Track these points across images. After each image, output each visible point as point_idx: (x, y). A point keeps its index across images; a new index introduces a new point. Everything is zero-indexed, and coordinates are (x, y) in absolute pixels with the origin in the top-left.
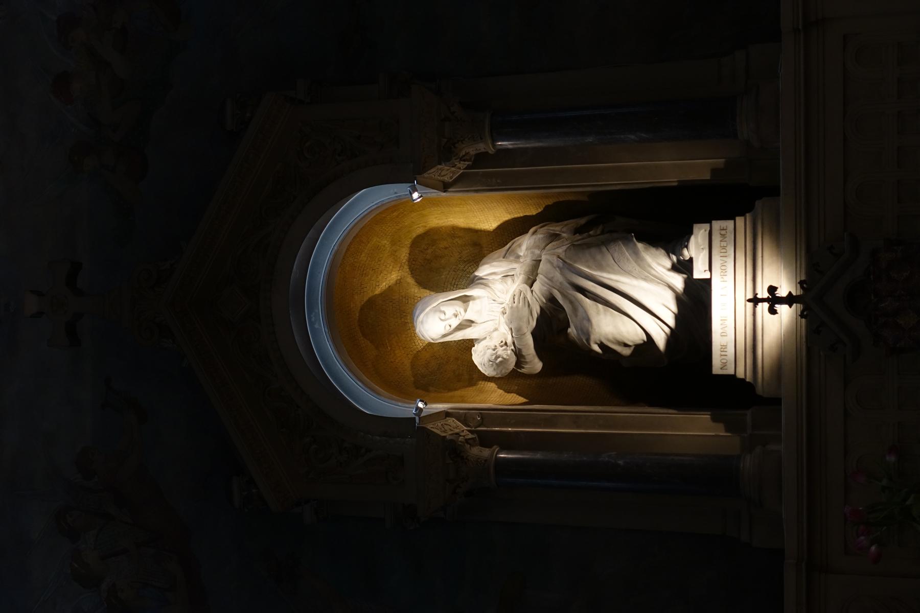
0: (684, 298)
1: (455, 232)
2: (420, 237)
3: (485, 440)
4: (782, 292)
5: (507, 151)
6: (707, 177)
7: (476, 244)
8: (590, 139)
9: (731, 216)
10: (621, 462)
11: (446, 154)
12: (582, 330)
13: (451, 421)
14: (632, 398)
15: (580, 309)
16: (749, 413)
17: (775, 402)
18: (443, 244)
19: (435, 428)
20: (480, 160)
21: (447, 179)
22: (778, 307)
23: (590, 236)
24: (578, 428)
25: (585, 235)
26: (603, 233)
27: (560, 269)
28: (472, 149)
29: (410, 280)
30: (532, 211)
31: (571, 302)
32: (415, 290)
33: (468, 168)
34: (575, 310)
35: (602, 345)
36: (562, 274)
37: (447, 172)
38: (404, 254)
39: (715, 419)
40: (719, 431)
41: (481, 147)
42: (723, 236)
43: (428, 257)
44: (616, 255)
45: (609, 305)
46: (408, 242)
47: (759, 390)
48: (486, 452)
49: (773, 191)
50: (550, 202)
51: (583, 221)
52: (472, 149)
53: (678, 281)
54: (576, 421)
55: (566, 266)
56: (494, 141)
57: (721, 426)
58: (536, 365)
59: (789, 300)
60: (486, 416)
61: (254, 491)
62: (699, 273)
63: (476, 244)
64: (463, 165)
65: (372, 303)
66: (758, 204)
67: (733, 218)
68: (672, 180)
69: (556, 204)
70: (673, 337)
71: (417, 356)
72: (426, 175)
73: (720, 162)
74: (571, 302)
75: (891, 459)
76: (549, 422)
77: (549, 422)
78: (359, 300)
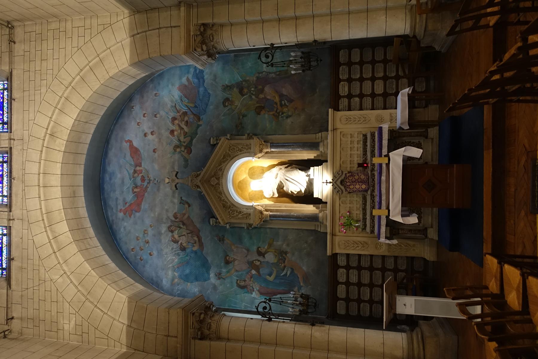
0: (308, 182)
1: (258, 167)
2: (251, 168)
3: (267, 210)
4: (328, 181)
5: (273, 151)
6: (313, 158)
7: (263, 170)
8: (290, 150)
9: (320, 166)
10: (295, 215)
11: (261, 151)
12: (287, 188)
13: (259, 206)
14: (296, 202)
15: (287, 184)
16: (320, 205)
17: (326, 203)
18: (255, 170)
19: (257, 207)
20: (267, 153)
21: (260, 156)
22: (327, 184)
23: (288, 169)
24: (286, 208)
25: (287, 169)
26: (291, 168)
27: (283, 175)
28: (265, 150)
29: (248, 177)
30: (276, 163)
31: (285, 182)
32: (249, 179)
33: (264, 154)
34: (286, 184)
35: (291, 192)
36: (283, 176)
37: (260, 155)
38: (247, 171)
39: (314, 206)
40: (315, 208)
41: (268, 150)
42: (316, 170)
43: (252, 172)
44: (295, 173)
45: (9, 244)
46: (248, 169)
47: (323, 201)
48: (267, 213)
49: (326, 161)
50: (280, 161)
51: (286, 166)
52: (265, 150)
53: (307, 178)
54: (286, 207)
55: (284, 175)
56: (270, 149)
57: (315, 208)
58: (276, 195)
59: (330, 183)
60: (266, 206)
61: (218, 221)
62: (311, 177)
63: (263, 170)
64: (263, 154)
65: (240, 182)
66: (323, 164)
67: (314, 167)
68: (306, 158)
69: (281, 162)
70: (306, 190)
71: (249, 193)
72: (256, 156)
73: (316, 155)
74: (285, 182)
75: (348, 214)
76: (280, 207)
77: (280, 207)
78: (238, 181)
